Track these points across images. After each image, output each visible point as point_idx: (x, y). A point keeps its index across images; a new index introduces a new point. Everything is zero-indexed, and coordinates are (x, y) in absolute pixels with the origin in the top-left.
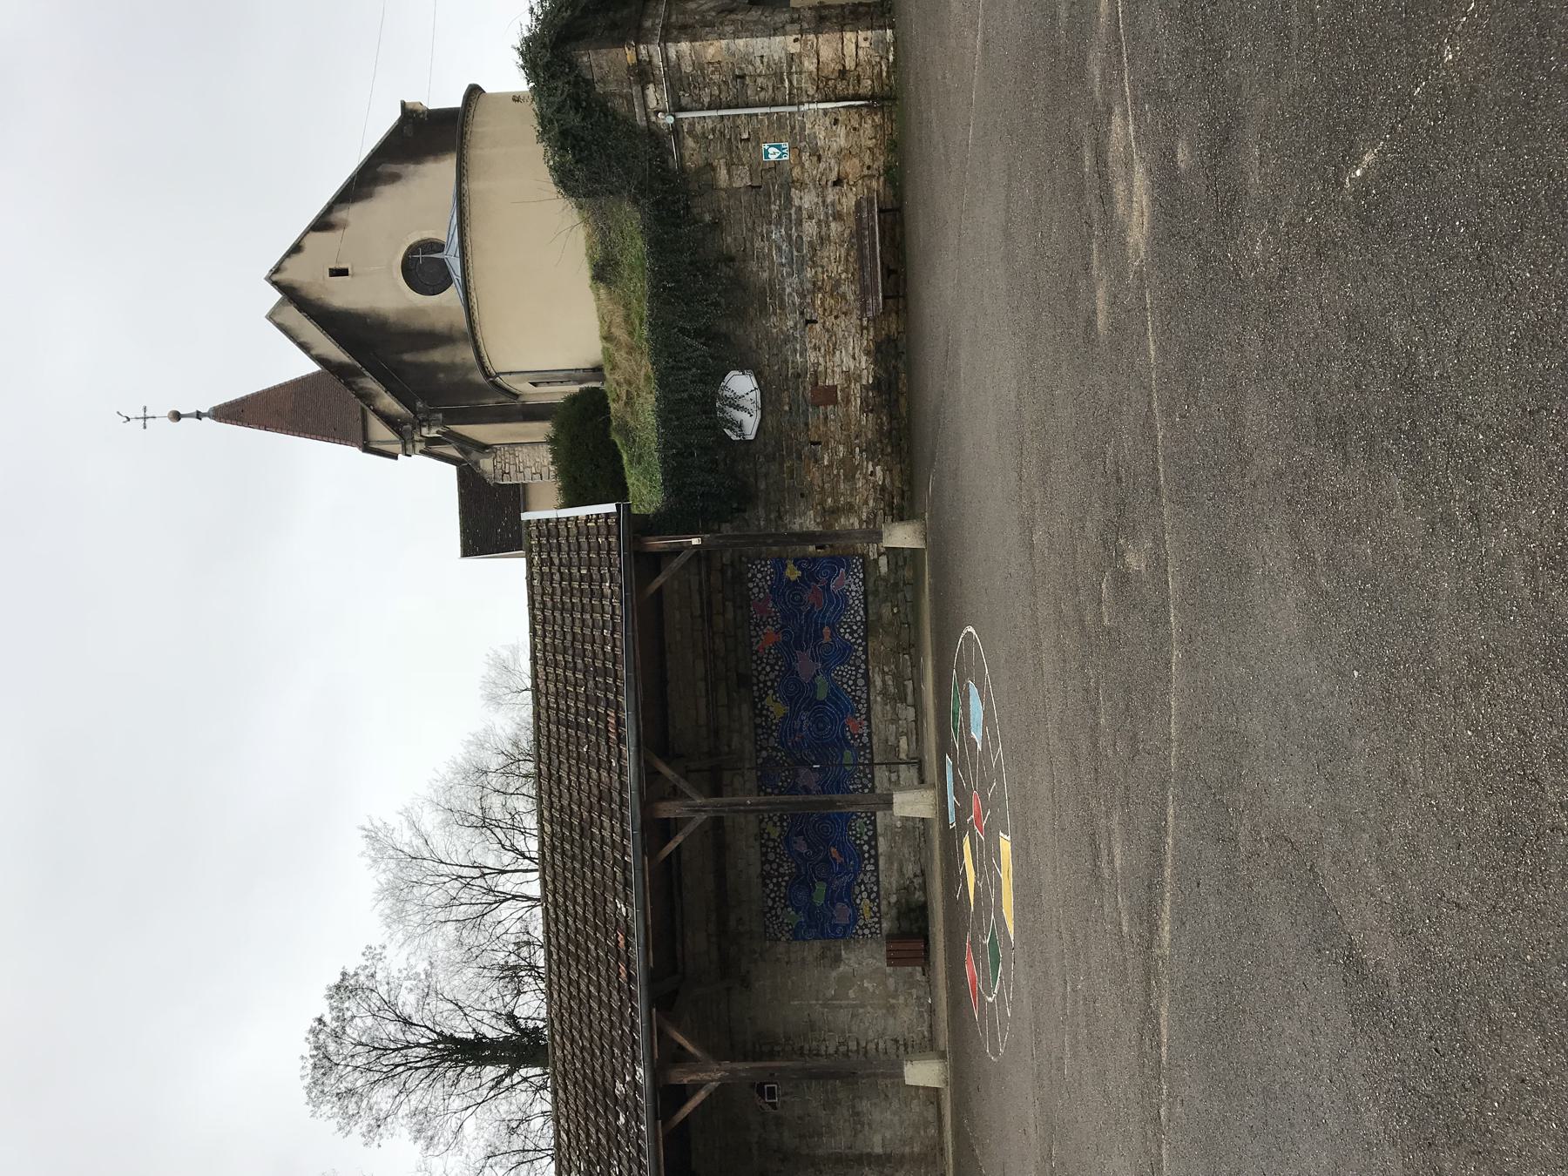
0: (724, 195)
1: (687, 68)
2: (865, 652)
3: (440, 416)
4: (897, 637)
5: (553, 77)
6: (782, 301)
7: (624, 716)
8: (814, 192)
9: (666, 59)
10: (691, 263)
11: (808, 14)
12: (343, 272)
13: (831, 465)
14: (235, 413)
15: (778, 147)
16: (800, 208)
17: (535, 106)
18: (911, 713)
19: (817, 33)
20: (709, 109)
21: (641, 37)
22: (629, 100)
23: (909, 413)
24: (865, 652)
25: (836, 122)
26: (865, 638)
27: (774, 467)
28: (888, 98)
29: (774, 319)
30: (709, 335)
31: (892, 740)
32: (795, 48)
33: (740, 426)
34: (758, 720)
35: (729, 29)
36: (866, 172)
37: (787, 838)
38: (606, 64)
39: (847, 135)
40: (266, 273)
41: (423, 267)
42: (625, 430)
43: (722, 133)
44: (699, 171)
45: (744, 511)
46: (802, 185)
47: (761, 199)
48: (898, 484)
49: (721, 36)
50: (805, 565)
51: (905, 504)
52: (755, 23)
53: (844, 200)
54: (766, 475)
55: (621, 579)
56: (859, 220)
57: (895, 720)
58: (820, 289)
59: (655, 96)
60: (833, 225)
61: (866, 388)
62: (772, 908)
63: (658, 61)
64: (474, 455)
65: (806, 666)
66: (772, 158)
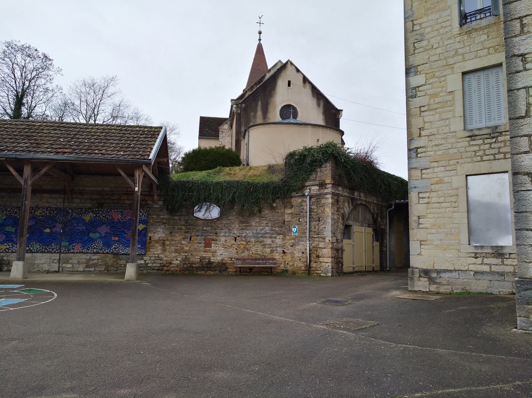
0: (282, 211)
1: (323, 201)
2: (107, 253)
3: (239, 112)
4: (112, 266)
5: (323, 154)
6: (244, 229)
7: (66, 155)
8: (281, 243)
9: (326, 194)
10: (259, 198)
11: (340, 245)
12: (289, 85)
13: (181, 244)
14: (260, 51)
15: (296, 232)
16: (276, 238)
17: (315, 147)
18: (81, 269)
19: (332, 248)
20: (310, 208)
21: (335, 185)
22: (314, 180)
23: (198, 274)
24: (107, 253)
25: (303, 253)
26: (112, 253)
27: (183, 223)
28: (309, 273)
29: (237, 226)
30: (233, 202)
31: (71, 261)
32: (327, 240)
33: (199, 211)
34: (84, 210)
35: (336, 217)
36: (286, 263)
37: (35, 218)
38: (326, 172)
39: (299, 257)
40: (291, 60)
41: (289, 111)
42: (219, 172)
43: (302, 212)
44: (290, 202)
45: (167, 210)
46: (284, 239)
47: (280, 224)
48: (172, 269)
49: (333, 214)
50: (143, 232)
51: (164, 272)
52: (337, 227)
53: (277, 254)
54: (180, 219)
55: (122, 158)
56: (269, 259)
57: (79, 263)
58: (247, 243)
59: (315, 189)
60: (269, 250)
61: (209, 259)
62: (6, 210)
63: (326, 191)
64: (229, 123)
65: (104, 230)
66: (293, 229)
